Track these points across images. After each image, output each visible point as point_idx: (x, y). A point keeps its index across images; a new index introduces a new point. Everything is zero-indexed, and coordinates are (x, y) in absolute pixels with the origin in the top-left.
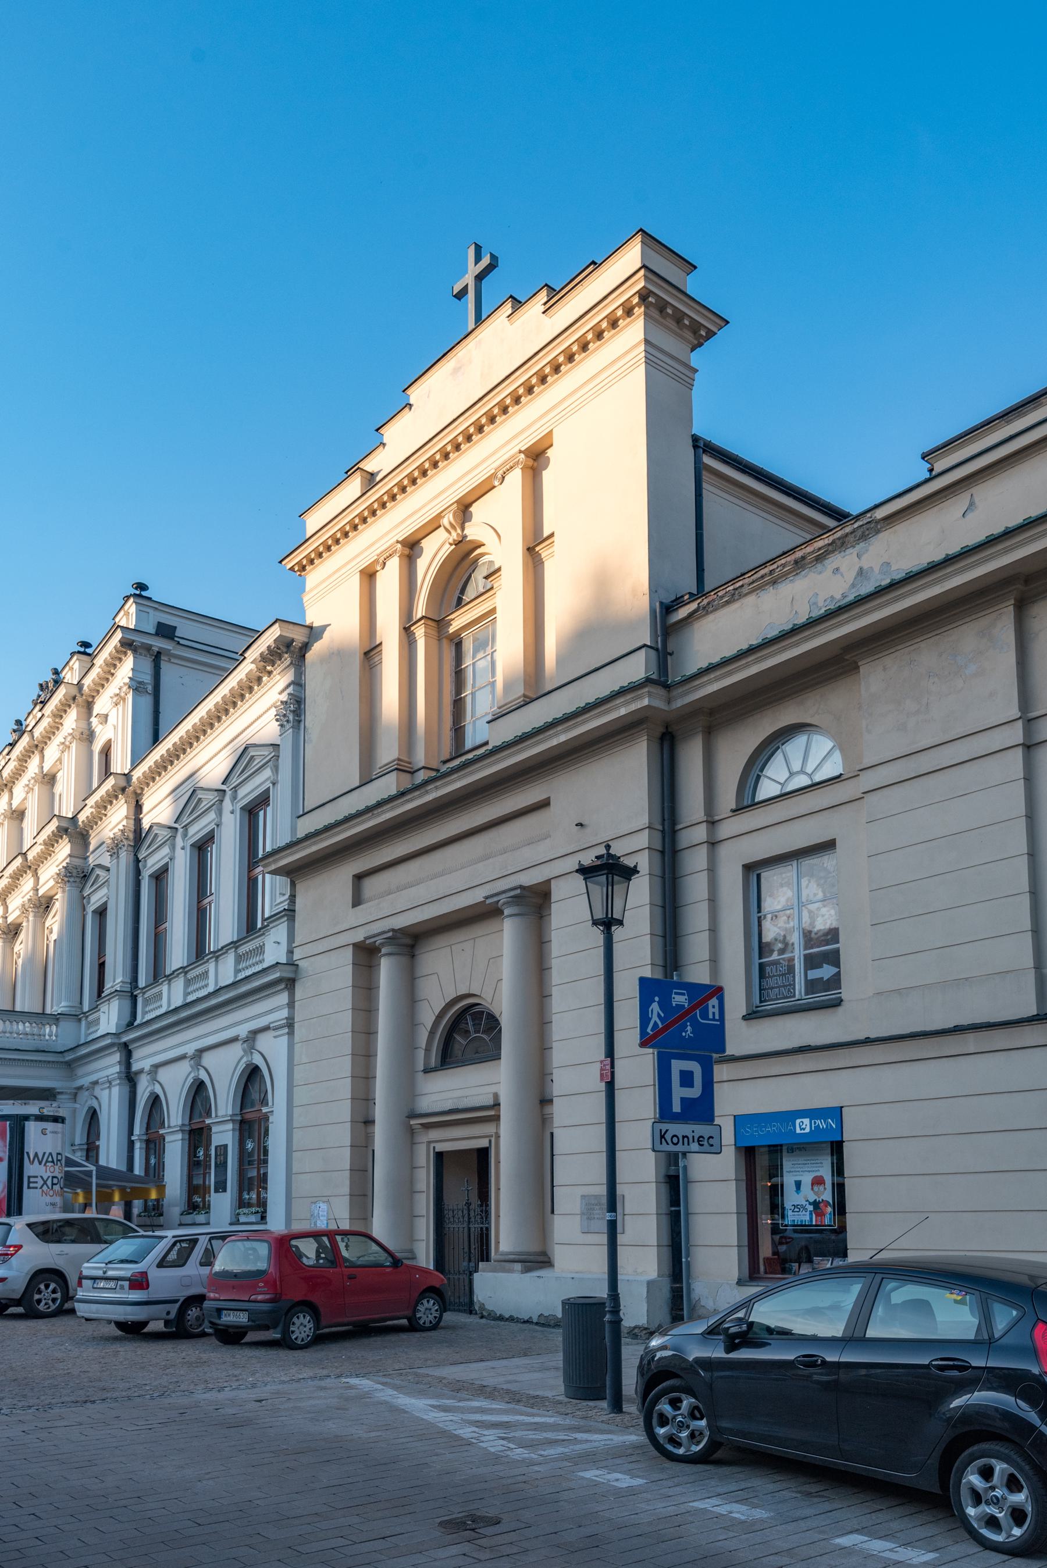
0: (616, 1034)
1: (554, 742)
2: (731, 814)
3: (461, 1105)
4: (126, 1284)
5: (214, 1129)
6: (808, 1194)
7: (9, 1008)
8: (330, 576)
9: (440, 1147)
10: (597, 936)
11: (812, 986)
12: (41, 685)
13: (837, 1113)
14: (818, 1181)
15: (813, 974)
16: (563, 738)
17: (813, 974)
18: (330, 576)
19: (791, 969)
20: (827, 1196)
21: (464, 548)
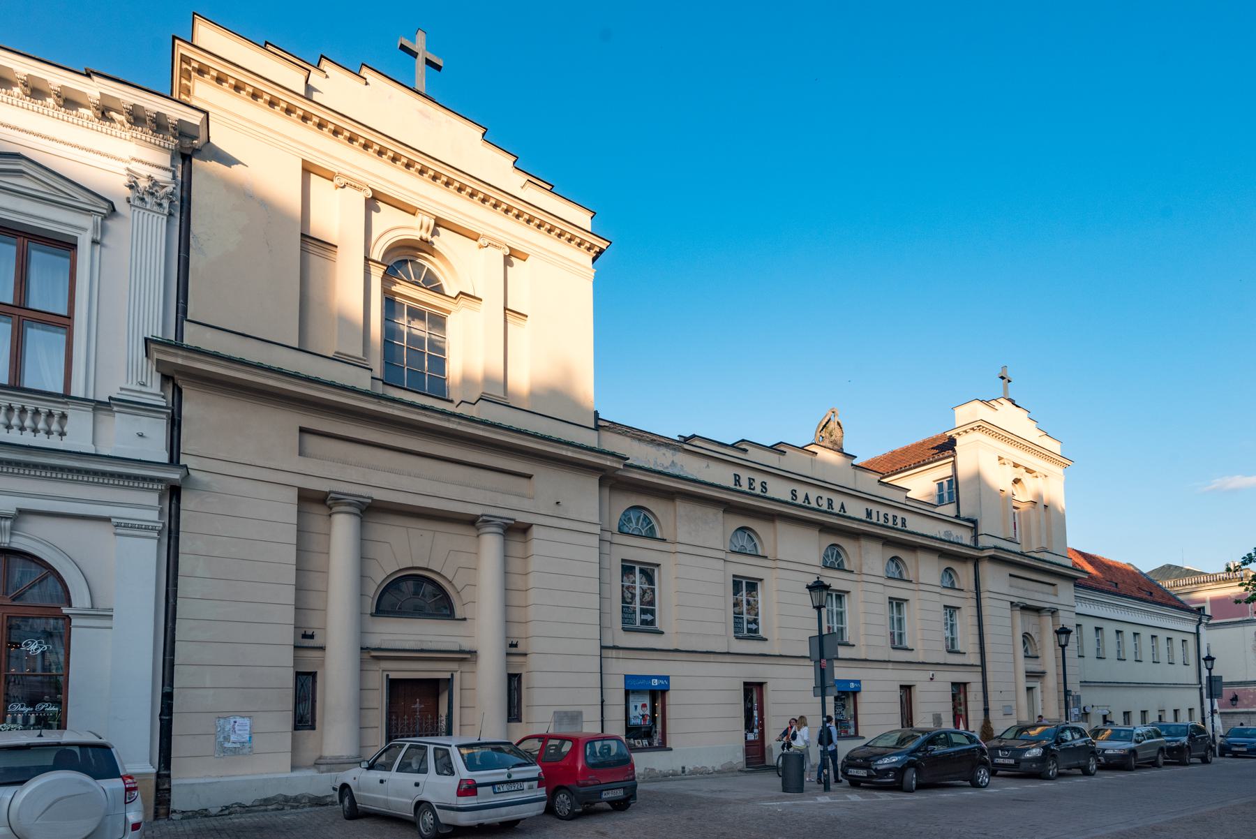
0: (180, 580)
1: (564, 453)
3: (425, 647)
4: (535, 783)
5: (74, 622)
6: (640, 711)
7: (61, 391)
8: (318, 151)
9: (393, 675)
10: (815, 612)
11: (644, 622)
12: (1213, 659)
13: (667, 678)
14: (644, 706)
15: (644, 617)
16: (570, 454)
17: (644, 617)
18: (318, 151)
19: (634, 612)
20: (648, 712)
21: (424, 247)
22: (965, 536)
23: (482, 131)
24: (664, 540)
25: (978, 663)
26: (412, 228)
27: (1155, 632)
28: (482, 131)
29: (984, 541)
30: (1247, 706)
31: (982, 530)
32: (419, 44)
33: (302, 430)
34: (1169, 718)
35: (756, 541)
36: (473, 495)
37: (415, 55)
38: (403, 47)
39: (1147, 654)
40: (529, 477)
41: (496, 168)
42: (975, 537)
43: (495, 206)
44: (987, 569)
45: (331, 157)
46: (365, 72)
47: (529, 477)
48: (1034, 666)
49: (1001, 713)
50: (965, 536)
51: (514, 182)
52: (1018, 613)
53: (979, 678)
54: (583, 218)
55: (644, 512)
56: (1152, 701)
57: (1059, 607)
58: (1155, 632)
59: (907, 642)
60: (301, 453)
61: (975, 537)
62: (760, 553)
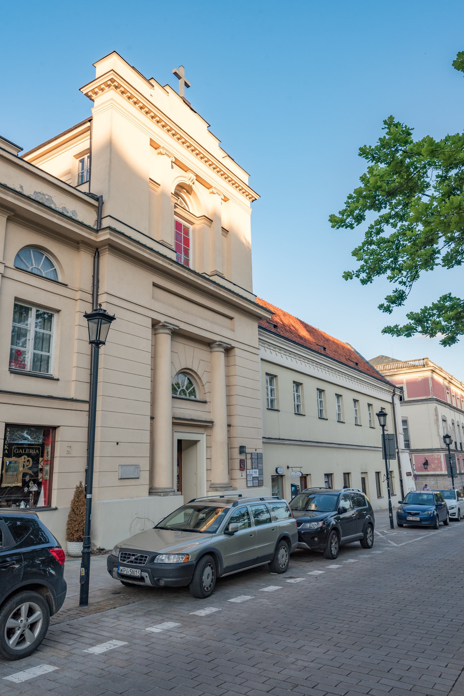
2: (14, 267)
18: (180, 153)
22: (87, 216)
23: (208, 126)
24: (66, 285)
25: (85, 396)
26: (187, 178)
27: (357, 397)
28: (208, 126)
29: (106, 223)
30: (434, 470)
31: (107, 211)
32: (181, 72)
33: (155, 285)
34: (338, 485)
35: (56, 266)
36: (216, 329)
37: (179, 78)
38: (175, 74)
39: (349, 416)
40: (231, 318)
41: (211, 145)
42: (100, 219)
43: (141, 108)
44: (108, 261)
45: (212, 178)
46: (167, 88)
47: (231, 318)
48: (189, 410)
49: (116, 476)
50: (87, 216)
51: (219, 154)
52: (165, 339)
53: (82, 419)
54: (245, 178)
55: (46, 254)
56: (338, 463)
57: (234, 344)
58: (357, 397)
59: (53, 371)
60: (153, 298)
61: (100, 219)
62: (60, 280)
